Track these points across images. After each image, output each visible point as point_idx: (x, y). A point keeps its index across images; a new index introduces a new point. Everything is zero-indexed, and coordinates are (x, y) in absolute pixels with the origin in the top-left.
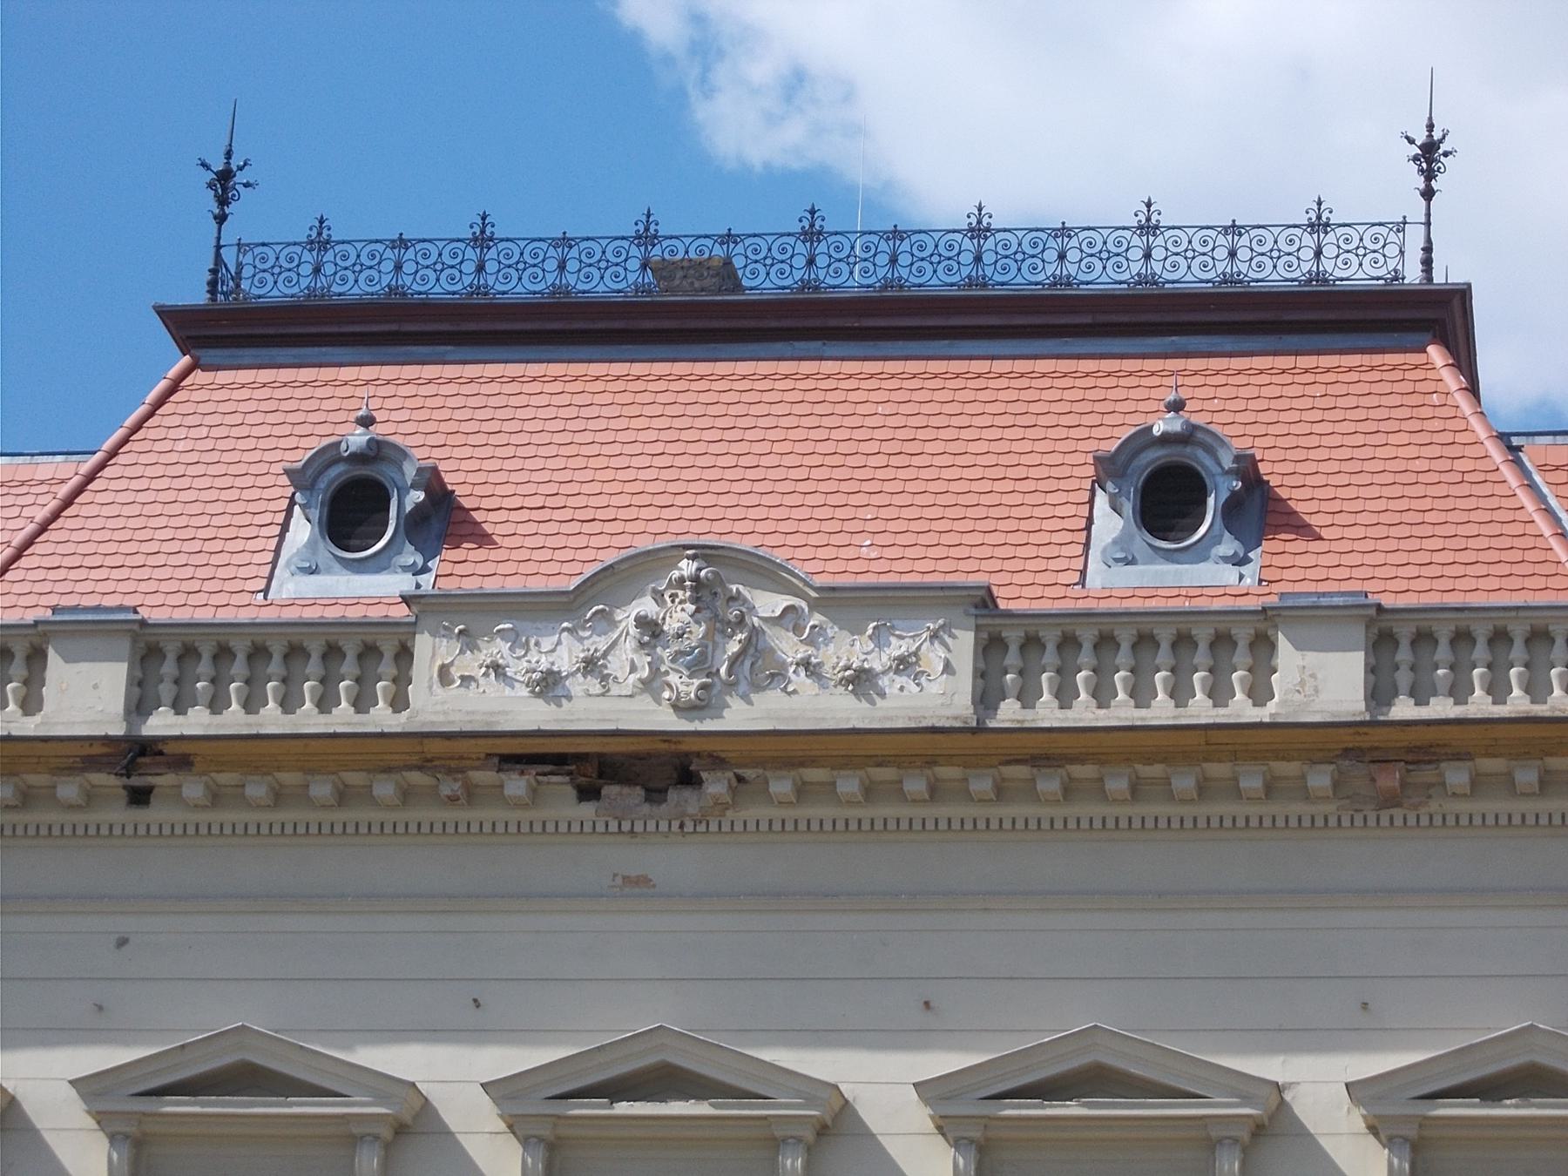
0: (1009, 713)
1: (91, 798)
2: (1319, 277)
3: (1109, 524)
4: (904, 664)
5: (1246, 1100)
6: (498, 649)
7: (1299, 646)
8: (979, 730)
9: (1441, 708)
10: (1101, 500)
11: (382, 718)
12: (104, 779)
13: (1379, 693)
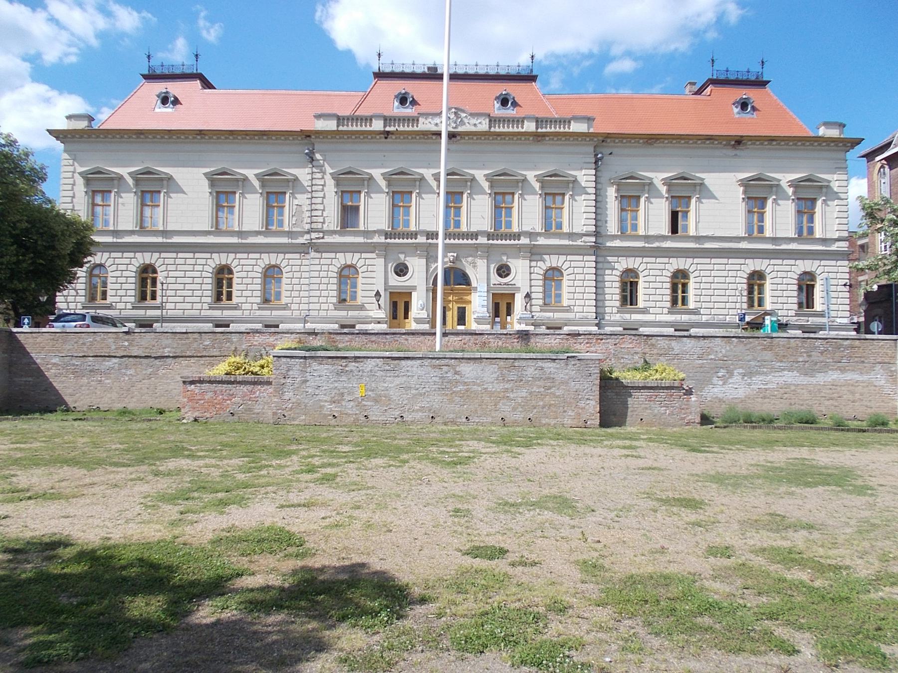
1: (380, 138)
3: (397, 104)
4: (480, 123)
6: (430, 120)
10: (495, 102)
11: (415, 128)
12: (382, 136)
13: (537, 128)
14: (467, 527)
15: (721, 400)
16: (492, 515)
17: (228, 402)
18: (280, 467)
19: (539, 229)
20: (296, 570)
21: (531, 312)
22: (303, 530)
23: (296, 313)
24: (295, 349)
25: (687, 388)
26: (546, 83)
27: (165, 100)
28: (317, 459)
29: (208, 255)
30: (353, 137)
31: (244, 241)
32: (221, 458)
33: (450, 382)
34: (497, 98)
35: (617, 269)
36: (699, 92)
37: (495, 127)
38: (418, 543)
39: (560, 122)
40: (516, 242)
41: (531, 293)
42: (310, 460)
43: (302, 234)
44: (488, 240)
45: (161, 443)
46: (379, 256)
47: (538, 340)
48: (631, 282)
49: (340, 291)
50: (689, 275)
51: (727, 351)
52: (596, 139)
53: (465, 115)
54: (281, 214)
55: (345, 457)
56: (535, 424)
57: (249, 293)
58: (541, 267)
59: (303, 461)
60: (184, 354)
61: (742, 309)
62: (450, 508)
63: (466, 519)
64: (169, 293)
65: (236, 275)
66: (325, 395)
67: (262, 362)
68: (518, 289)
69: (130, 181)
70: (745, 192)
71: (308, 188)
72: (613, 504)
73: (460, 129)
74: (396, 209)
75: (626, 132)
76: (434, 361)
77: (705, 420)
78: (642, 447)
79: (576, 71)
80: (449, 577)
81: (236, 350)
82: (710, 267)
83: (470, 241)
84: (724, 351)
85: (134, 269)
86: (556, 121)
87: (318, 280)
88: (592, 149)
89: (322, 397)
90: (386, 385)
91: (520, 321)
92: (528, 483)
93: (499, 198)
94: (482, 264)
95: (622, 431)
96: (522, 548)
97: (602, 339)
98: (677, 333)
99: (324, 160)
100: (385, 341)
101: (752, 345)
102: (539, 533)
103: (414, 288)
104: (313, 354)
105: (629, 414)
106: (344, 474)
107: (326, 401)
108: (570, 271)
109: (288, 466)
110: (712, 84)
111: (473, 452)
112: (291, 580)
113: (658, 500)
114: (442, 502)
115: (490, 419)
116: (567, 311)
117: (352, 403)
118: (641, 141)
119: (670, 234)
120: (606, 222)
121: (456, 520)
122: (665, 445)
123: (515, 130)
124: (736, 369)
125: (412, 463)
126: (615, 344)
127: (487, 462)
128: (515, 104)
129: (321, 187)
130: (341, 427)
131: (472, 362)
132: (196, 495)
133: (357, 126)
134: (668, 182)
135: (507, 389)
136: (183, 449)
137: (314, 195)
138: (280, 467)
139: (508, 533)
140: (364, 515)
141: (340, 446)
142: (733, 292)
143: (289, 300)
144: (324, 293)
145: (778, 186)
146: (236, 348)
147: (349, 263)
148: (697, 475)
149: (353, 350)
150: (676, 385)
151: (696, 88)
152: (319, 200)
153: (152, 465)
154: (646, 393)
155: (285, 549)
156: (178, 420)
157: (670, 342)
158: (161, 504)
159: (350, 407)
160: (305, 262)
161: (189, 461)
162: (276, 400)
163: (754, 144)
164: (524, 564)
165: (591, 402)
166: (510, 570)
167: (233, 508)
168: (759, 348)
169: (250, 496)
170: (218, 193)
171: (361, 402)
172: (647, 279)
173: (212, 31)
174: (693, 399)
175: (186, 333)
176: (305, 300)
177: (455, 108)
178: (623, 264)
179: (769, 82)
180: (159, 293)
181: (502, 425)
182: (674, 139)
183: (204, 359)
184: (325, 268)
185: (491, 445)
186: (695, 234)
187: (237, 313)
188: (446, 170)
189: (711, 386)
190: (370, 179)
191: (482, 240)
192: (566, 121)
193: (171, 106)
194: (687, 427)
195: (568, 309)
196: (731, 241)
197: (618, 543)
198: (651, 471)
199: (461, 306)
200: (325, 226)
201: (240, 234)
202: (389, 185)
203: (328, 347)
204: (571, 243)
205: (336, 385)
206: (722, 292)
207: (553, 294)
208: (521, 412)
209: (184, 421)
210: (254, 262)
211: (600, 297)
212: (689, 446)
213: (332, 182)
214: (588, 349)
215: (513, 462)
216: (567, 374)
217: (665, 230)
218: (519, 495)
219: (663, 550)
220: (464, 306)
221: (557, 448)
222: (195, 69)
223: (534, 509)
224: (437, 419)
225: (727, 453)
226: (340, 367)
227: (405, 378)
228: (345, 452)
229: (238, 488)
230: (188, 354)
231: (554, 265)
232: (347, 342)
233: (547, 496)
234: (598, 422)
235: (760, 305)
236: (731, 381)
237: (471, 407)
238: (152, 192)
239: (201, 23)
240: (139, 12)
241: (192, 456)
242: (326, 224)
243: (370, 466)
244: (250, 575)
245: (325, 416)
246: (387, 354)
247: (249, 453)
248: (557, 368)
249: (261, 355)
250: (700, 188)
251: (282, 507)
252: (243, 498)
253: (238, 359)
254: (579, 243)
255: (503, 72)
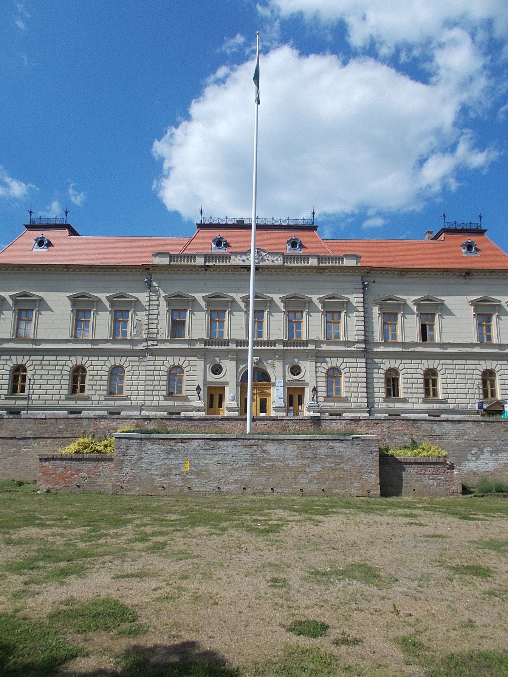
0: (286, 264)
1: (202, 271)
2: (40, 223)
4: (276, 260)
5: (347, 300)
7: (311, 258)
8: (169, 265)
9: (324, 265)
10: (287, 245)
11: (228, 263)
12: (203, 269)
13: (319, 263)
14: (287, 600)
15: (475, 473)
16: (307, 585)
17: (76, 476)
18: (117, 535)
19: (322, 338)
20: (129, 651)
21: (317, 402)
22: (135, 603)
23: (134, 403)
24: (133, 432)
25: (450, 464)
26: (321, 234)
27: (41, 243)
28: (148, 527)
29: (67, 358)
30: (182, 270)
31: (95, 347)
32: (66, 527)
33: (258, 459)
34: (288, 242)
35: (382, 369)
36: (436, 238)
37: (287, 263)
38: (244, 618)
39: (336, 258)
40: (305, 348)
41: (317, 387)
42: (142, 528)
43: (141, 342)
44: (284, 347)
45: (16, 513)
46: (199, 359)
47: (327, 424)
48: (393, 379)
49: (169, 386)
50: (437, 373)
51: (477, 433)
52: (362, 271)
53: (265, 254)
54: (125, 327)
55: (173, 525)
56: (327, 494)
57: (98, 387)
58: (324, 367)
59: (137, 529)
60: (42, 436)
61: (480, 399)
62: (268, 578)
63: (285, 589)
64: (35, 387)
65: (88, 373)
66: (156, 470)
67: (106, 442)
68: (307, 384)
69: (11, 302)
70: (475, 310)
71: (146, 307)
72: (412, 573)
73: (261, 264)
74: (213, 323)
75: (386, 266)
76: (246, 441)
77: (465, 490)
78: (422, 516)
79: (342, 226)
80: (277, 659)
81: (85, 432)
82: (453, 367)
83: (270, 348)
84: (475, 433)
85: (9, 369)
86: (332, 258)
87: (152, 378)
88: (361, 278)
89: (153, 472)
90: (206, 462)
91: (309, 409)
92: (332, 551)
93: (291, 314)
94: (279, 365)
95: (400, 500)
96: (341, 623)
97: (378, 424)
98: (391, 418)
99: (159, 287)
100: (205, 425)
101: (496, 428)
102: (354, 606)
103: (227, 383)
104: (147, 436)
105: (404, 485)
106: (172, 542)
107: (157, 475)
108: (347, 370)
109: (123, 535)
110: (445, 232)
111: (280, 520)
112: (123, 664)
113: (451, 568)
114: (261, 572)
115: (291, 490)
116: (345, 401)
117: (178, 477)
118: (396, 273)
119: (421, 342)
120: (373, 332)
121: (275, 591)
122: (440, 513)
123: (303, 264)
124: (485, 447)
125: (231, 531)
126: (388, 428)
127: (294, 530)
128: (302, 246)
129: (156, 307)
130: (169, 496)
131: (276, 442)
132: (41, 564)
133: (184, 261)
134: (416, 303)
135: (305, 465)
136: (35, 518)
137: (151, 312)
138: (117, 535)
139: (325, 605)
140: (191, 586)
141: (169, 515)
142: (471, 386)
143: (129, 393)
144: (157, 388)
145: (500, 305)
146: (85, 431)
147: (176, 364)
148: (475, 542)
149: (180, 432)
150: (441, 461)
151: (433, 235)
152: (155, 317)
153: (5, 533)
154: (416, 468)
155: (119, 625)
156: (34, 491)
157: (432, 425)
158: (8, 573)
159: (176, 480)
160: (143, 363)
161: (38, 530)
162: (116, 474)
163: (479, 275)
164: (345, 642)
165: (373, 475)
166: (333, 649)
167: (73, 579)
168: (502, 430)
169: (89, 566)
170: (77, 311)
171: (185, 476)
172: (405, 376)
173: (78, 197)
174: (455, 473)
175: (45, 419)
176: (141, 393)
177: (258, 249)
178: (387, 364)
179: (486, 230)
180: (27, 387)
181: (301, 495)
182: (419, 271)
183: (58, 440)
184: (158, 368)
185: (294, 513)
186: (440, 342)
187: (89, 403)
188: (254, 293)
189: (467, 462)
190: (193, 300)
191: (279, 347)
192: (341, 258)
193: (45, 247)
194: (452, 497)
195: (346, 400)
196: (467, 347)
197: (429, 615)
198: (436, 539)
199: (263, 397)
200: (159, 336)
201: (93, 341)
202: (208, 305)
203: (160, 430)
204: (346, 349)
205: (166, 461)
206: (463, 386)
207: (334, 388)
208: (316, 484)
209: (39, 492)
210: (103, 363)
211: (370, 390)
212: (459, 514)
213: (165, 303)
214: (367, 431)
215: (316, 530)
216: (353, 452)
217: (417, 338)
218: (327, 564)
219: (471, 624)
220: (265, 397)
221: (351, 517)
222: (65, 221)
223: (343, 579)
224: (248, 490)
225: (493, 521)
226: (169, 447)
227: (222, 456)
228: (172, 521)
229: (79, 557)
230: (46, 435)
231: (334, 365)
232: (175, 426)
233: (352, 565)
234: (378, 492)
235: (492, 396)
236: (482, 457)
237: (275, 480)
238: (27, 310)
239: (71, 191)
240: (26, 183)
241: (42, 525)
242: (160, 335)
243: (194, 534)
244: (84, 656)
245: (156, 487)
246: (208, 436)
247: (91, 522)
248: (345, 447)
249: (106, 437)
250: (442, 308)
251: (117, 577)
252: (82, 568)
253: (86, 440)
254: (353, 348)
255: (292, 224)
